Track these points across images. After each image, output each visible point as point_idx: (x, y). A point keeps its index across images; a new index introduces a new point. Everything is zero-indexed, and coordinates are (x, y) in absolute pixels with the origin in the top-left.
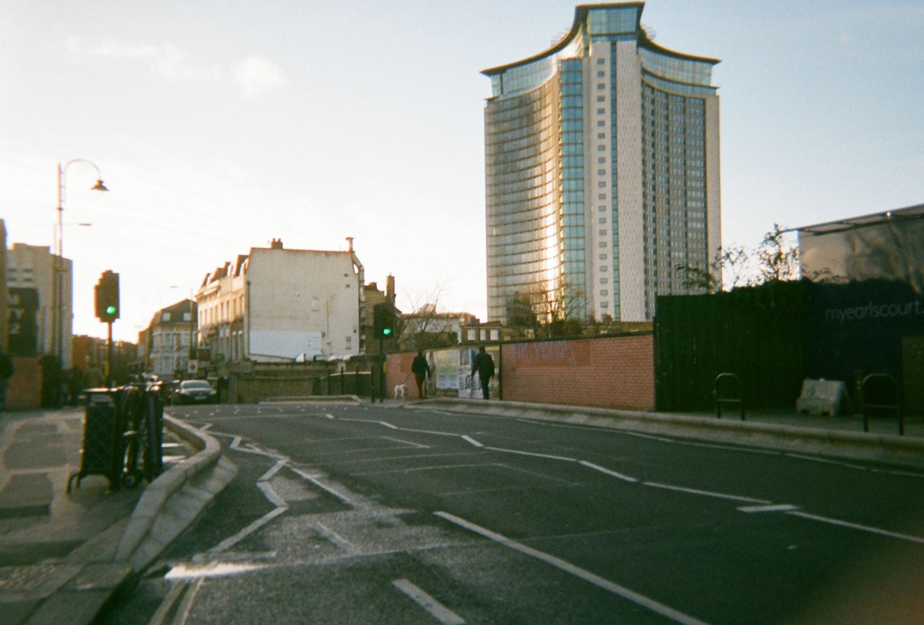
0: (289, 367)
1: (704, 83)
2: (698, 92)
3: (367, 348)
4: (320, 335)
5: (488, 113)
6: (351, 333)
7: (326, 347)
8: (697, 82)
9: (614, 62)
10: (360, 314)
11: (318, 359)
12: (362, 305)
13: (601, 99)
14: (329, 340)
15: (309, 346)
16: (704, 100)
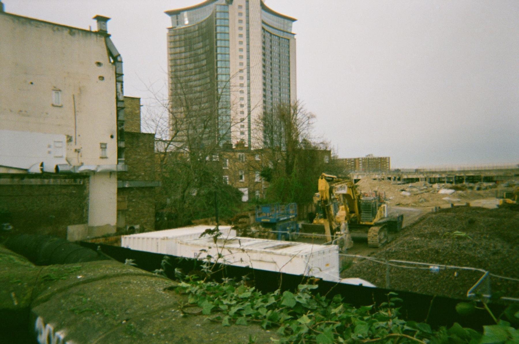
0: (16, 180)
1: (289, 31)
2: (285, 36)
3: (126, 158)
4: (65, 139)
5: (170, 36)
6: (107, 139)
7: (74, 156)
8: (285, 30)
9: (248, 9)
10: (118, 116)
11: (61, 169)
12: (120, 105)
13: (241, 28)
14: (77, 147)
15: (49, 152)
16: (289, 40)
